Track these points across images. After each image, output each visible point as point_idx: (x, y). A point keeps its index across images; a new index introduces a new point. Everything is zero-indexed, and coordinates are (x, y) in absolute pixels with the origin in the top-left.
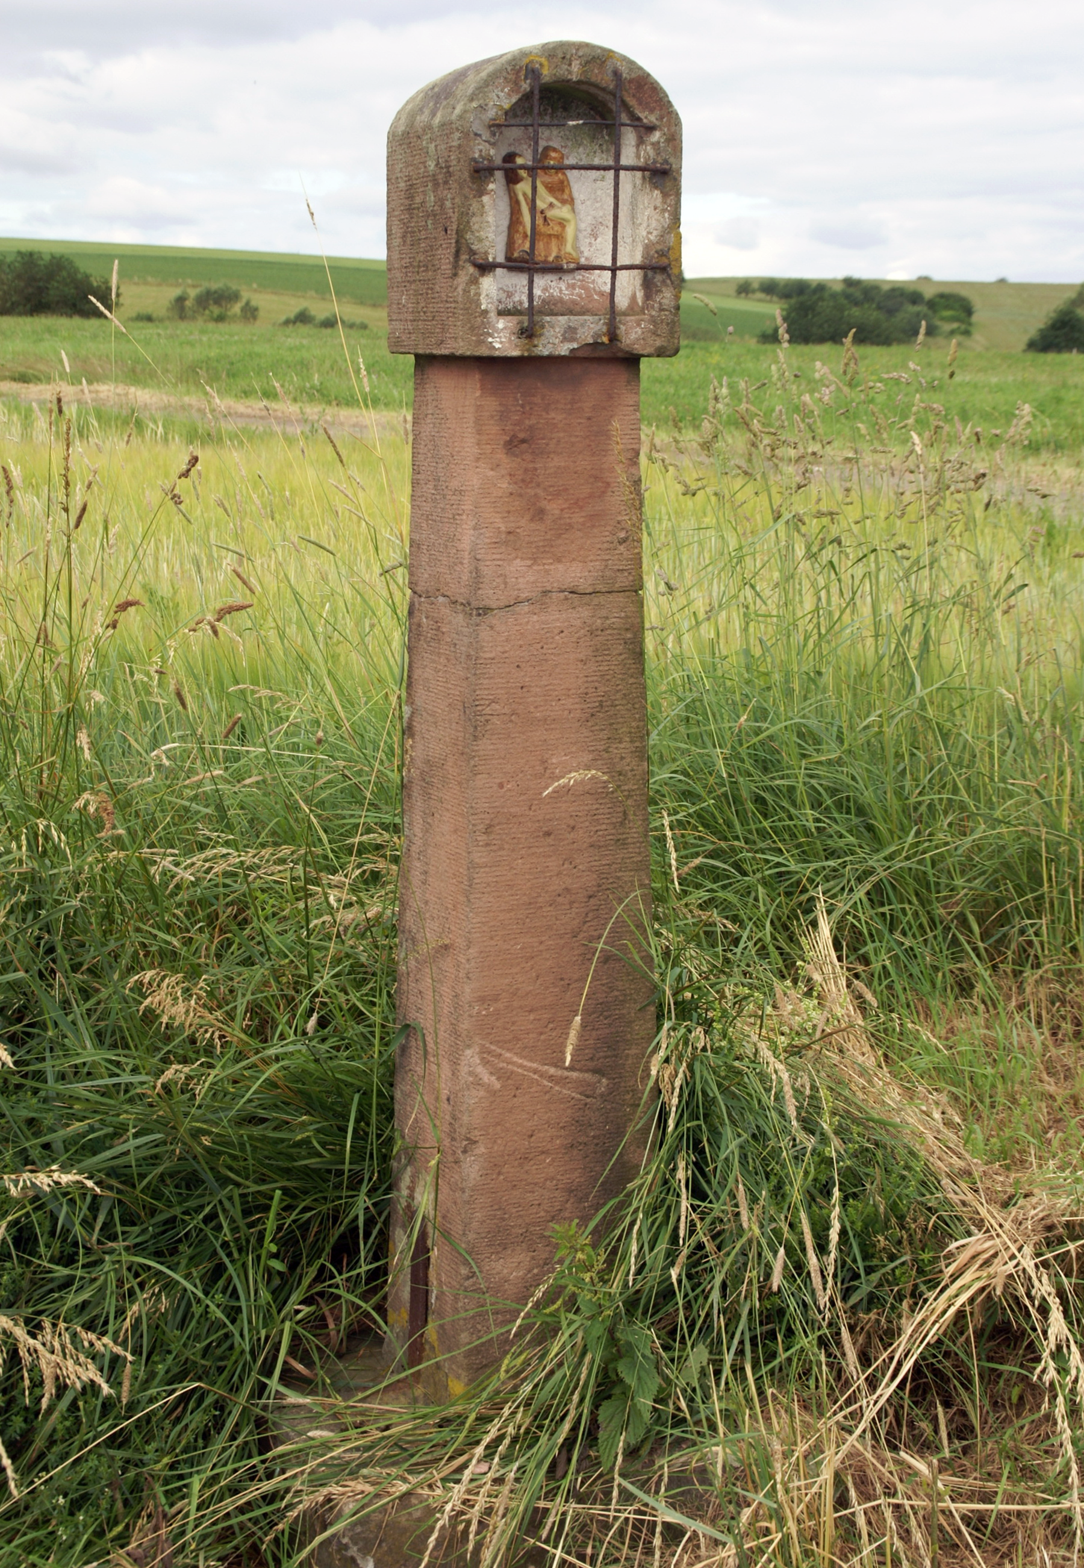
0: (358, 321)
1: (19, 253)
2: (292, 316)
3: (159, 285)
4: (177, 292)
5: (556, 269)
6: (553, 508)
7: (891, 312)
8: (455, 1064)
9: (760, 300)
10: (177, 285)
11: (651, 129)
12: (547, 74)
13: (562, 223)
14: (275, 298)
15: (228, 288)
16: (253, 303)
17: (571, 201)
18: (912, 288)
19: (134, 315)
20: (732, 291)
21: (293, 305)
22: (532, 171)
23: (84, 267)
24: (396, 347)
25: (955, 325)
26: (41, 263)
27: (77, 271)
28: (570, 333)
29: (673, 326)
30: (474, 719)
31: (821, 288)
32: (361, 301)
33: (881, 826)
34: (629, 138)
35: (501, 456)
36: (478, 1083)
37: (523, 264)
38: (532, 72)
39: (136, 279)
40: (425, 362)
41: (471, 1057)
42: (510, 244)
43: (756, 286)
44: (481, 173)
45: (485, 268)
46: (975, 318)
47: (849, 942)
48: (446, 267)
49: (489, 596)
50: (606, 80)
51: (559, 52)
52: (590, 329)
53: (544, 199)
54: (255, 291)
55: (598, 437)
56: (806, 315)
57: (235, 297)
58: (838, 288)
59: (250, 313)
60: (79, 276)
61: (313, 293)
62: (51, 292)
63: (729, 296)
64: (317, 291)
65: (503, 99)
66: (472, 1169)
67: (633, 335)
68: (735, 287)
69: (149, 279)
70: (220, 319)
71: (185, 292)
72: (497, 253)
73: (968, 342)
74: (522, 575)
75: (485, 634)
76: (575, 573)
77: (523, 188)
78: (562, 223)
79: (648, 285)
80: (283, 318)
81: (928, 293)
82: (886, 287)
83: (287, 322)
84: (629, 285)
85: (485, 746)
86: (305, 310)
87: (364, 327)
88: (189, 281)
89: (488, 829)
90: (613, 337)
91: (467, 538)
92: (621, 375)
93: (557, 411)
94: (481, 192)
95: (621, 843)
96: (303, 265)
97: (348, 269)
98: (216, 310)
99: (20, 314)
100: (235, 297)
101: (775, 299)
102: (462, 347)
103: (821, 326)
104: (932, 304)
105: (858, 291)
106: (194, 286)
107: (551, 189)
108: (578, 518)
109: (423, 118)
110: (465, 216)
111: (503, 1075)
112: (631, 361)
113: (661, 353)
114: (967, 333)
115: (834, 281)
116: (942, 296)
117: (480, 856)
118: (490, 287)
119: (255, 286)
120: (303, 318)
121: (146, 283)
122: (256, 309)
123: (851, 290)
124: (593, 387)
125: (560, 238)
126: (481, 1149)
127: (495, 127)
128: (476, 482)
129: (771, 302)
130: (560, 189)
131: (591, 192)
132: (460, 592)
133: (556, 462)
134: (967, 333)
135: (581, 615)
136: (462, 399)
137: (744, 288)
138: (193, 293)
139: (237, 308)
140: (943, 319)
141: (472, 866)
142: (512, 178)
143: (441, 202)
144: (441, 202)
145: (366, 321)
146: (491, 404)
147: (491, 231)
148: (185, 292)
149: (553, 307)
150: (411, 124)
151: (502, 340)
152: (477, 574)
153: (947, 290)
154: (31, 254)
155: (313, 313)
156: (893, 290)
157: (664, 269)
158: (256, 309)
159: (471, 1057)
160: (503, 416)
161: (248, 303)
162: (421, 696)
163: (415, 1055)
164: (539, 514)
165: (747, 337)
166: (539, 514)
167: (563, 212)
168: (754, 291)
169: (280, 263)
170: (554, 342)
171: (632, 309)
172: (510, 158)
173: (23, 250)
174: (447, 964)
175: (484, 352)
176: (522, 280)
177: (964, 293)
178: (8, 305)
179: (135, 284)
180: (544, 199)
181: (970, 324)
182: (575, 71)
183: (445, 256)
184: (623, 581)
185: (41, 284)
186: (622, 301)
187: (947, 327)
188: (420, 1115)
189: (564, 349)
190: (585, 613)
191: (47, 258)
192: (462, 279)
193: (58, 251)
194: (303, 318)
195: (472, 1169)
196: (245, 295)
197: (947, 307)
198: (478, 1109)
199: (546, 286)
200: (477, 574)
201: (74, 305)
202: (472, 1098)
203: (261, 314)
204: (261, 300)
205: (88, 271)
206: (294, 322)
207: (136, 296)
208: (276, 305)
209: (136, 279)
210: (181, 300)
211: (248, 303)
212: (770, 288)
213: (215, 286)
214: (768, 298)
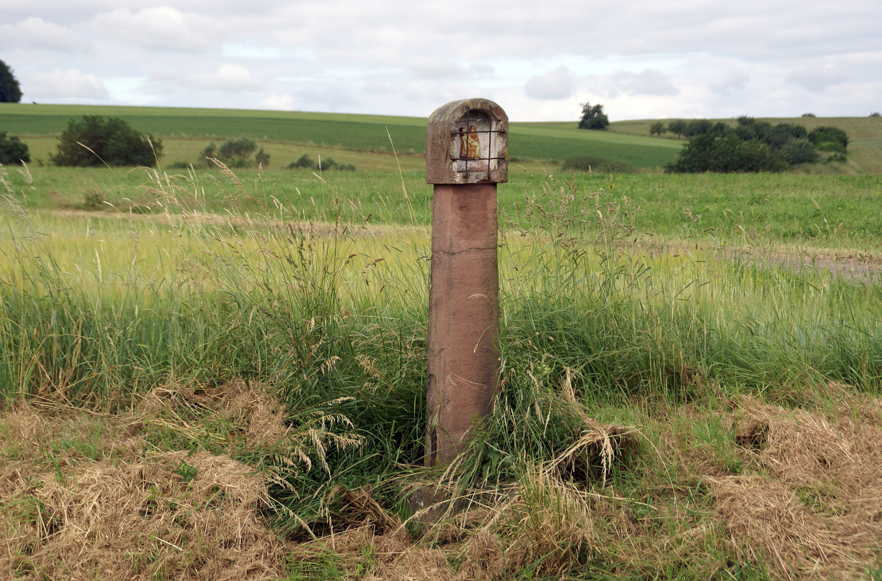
0: (347, 164)
1: (85, 117)
2: (295, 161)
3: (191, 139)
4: (206, 144)
5: (473, 159)
6: (472, 225)
7: (778, 145)
8: (444, 380)
9: (670, 138)
10: (206, 139)
11: (500, 121)
12: (471, 107)
13: (475, 147)
14: (281, 146)
15: (246, 141)
16: (266, 152)
17: (478, 140)
18: (796, 124)
19: (173, 163)
20: (647, 132)
21: (296, 152)
22: (467, 133)
23: (135, 126)
24: (429, 182)
25: (833, 154)
26: (102, 124)
27: (129, 129)
28: (477, 177)
29: (506, 174)
30: (450, 284)
31: (720, 127)
32: (349, 148)
33: (592, 348)
34: (494, 123)
35: (458, 211)
36: (451, 384)
37: (464, 158)
38: (467, 107)
39: (173, 135)
40: (437, 186)
41: (449, 377)
42: (461, 153)
43: (666, 126)
44: (453, 135)
45: (454, 160)
46: (849, 147)
47: (577, 383)
48: (443, 160)
49: (455, 250)
50: (488, 108)
51: (474, 101)
52: (483, 176)
53: (471, 140)
54: (266, 141)
55: (484, 206)
56: (705, 150)
57: (250, 147)
58: (735, 126)
59: (264, 159)
60: (131, 134)
61: (311, 142)
62: (109, 147)
63: (644, 135)
64: (314, 141)
65: (459, 114)
66: (449, 408)
67: (495, 177)
68: (649, 128)
69: (183, 135)
70: (240, 165)
71: (213, 145)
72: (457, 156)
73: (843, 167)
74: (464, 244)
75: (453, 260)
76: (478, 243)
77: (465, 137)
78: (475, 147)
79: (499, 163)
80: (289, 163)
81: (810, 127)
82: (775, 124)
83: (292, 166)
84: (493, 164)
85: (453, 291)
86: (305, 156)
87: (352, 168)
88: (214, 136)
89: (454, 314)
90: (489, 178)
91: (449, 234)
92: (491, 189)
93: (473, 197)
94: (453, 140)
95: (491, 319)
96: (303, 120)
97: (339, 122)
98: (236, 158)
99: (84, 166)
100: (250, 147)
101: (682, 136)
102: (448, 182)
103: (716, 158)
104: (813, 137)
105: (750, 128)
106: (218, 139)
107: (472, 137)
108: (479, 228)
109: (438, 119)
110: (449, 146)
111: (458, 383)
112: (494, 184)
113: (502, 182)
114: (843, 160)
115: (732, 120)
116: (821, 130)
117: (451, 322)
118: (455, 165)
119: (266, 138)
120: (304, 163)
121: (181, 138)
122: (268, 156)
123: (746, 127)
124: (484, 192)
125: (475, 151)
126: (451, 403)
127: (457, 122)
128: (451, 218)
129: (679, 139)
130: (475, 137)
131: (483, 138)
132: (446, 249)
133: (473, 212)
134: (843, 160)
135: (479, 255)
136: (447, 196)
137: (657, 128)
138: (219, 145)
139: (253, 156)
140: (822, 149)
141: (449, 324)
142: (462, 135)
143: (442, 142)
144: (442, 142)
145: (353, 164)
146: (456, 197)
147: (456, 151)
148: (213, 145)
149: (472, 170)
150: (434, 120)
151: (458, 179)
152: (451, 244)
153: (825, 125)
154: (94, 118)
155: (311, 158)
156: (780, 126)
157: (503, 159)
158: (268, 156)
159: (449, 377)
160: (459, 200)
161: (261, 152)
162: (435, 280)
163: (432, 383)
164: (469, 227)
165: (658, 168)
166: (469, 227)
167: (476, 143)
168: (664, 131)
169: (286, 120)
170: (473, 180)
171: (494, 170)
172: (461, 130)
173: (88, 114)
174: (442, 354)
175: (453, 183)
176: (464, 162)
177: (840, 127)
178: (76, 158)
179: (172, 139)
180: (471, 140)
181: (846, 153)
182: (479, 107)
183: (443, 157)
184: (492, 245)
185: (101, 141)
186: (492, 168)
187: (826, 155)
188: (434, 398)
189: (475, 182)
190: (481, 254)
191: (106, 120)
192: (448, 163)
193: (113, 114)
194: (304, 163)
195: (449, 408)
196: (259, 145)
197: (825, 139)
198: (450, 394)
199: (471, 164)
200: (451, 244)
201: (127, 157)
202: (449, 388)
203: (272, 160)
204: (271, 149)
205: (138, 130)
206: (297, 166)
207: (173, 148)
208: (283, 152)
209: (173, 135)
210: (209, 151)
211: (261, 152)
212: (678, 127)
213: (235, 139)
214: (677, 136)
